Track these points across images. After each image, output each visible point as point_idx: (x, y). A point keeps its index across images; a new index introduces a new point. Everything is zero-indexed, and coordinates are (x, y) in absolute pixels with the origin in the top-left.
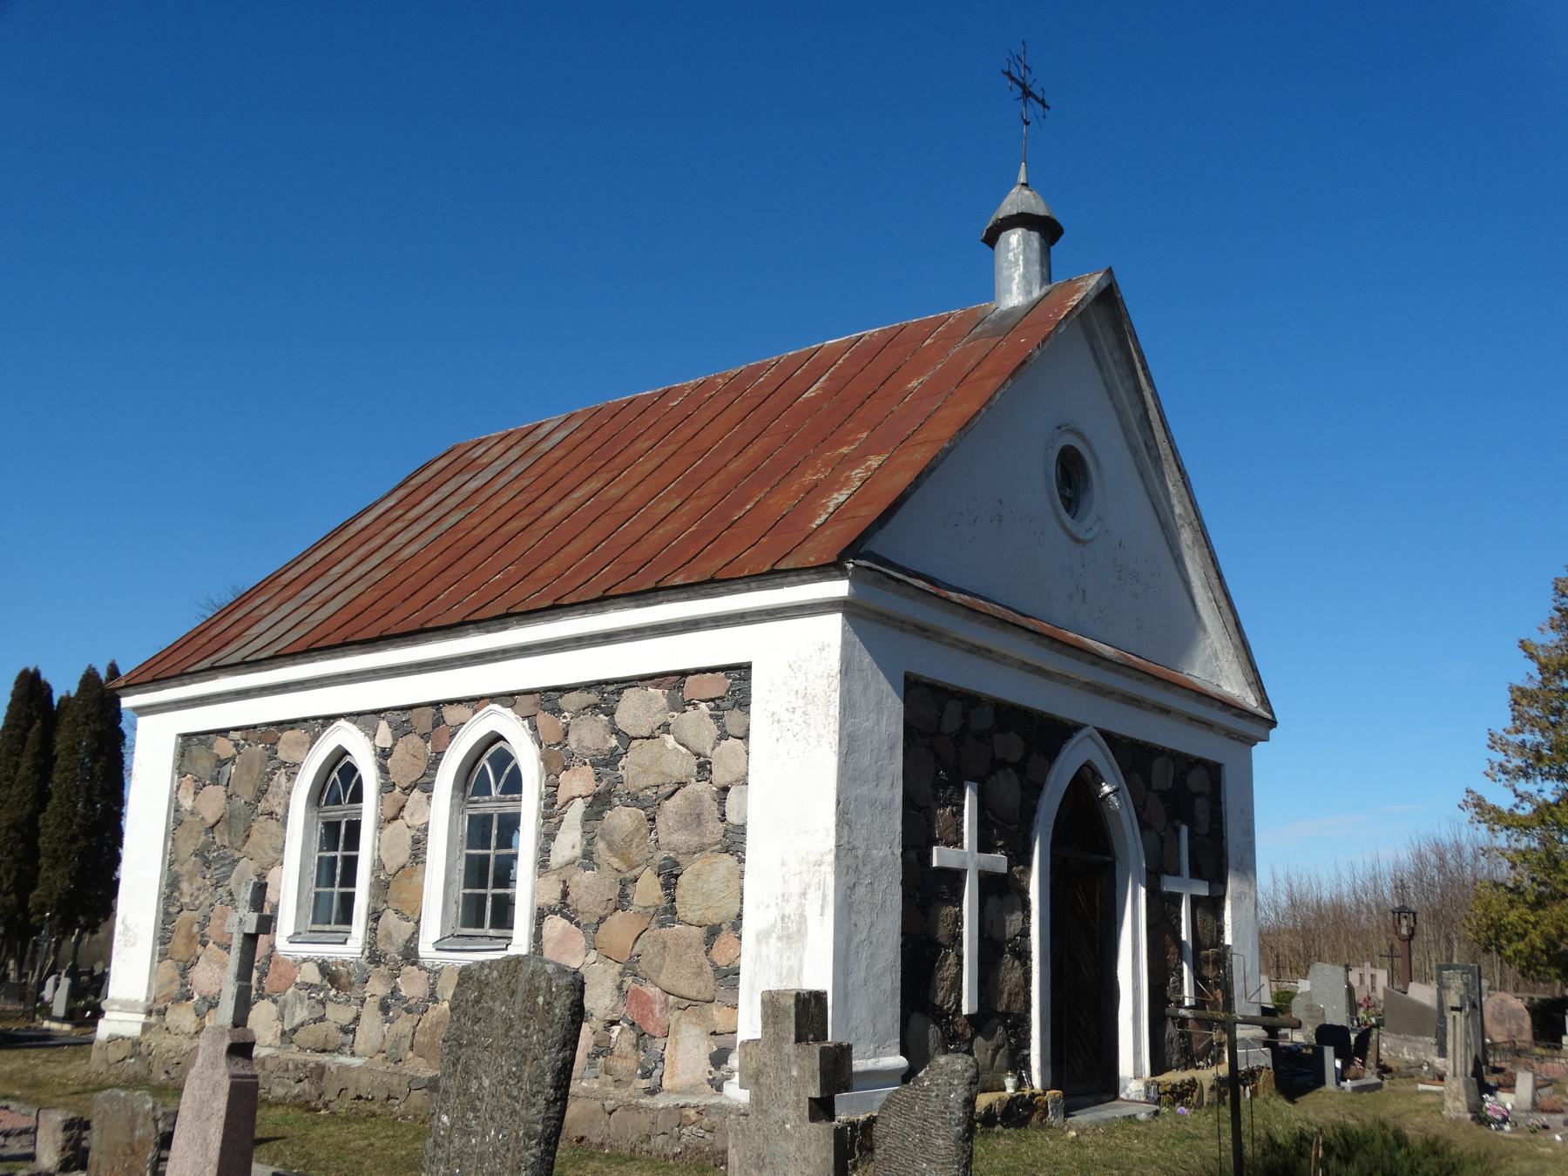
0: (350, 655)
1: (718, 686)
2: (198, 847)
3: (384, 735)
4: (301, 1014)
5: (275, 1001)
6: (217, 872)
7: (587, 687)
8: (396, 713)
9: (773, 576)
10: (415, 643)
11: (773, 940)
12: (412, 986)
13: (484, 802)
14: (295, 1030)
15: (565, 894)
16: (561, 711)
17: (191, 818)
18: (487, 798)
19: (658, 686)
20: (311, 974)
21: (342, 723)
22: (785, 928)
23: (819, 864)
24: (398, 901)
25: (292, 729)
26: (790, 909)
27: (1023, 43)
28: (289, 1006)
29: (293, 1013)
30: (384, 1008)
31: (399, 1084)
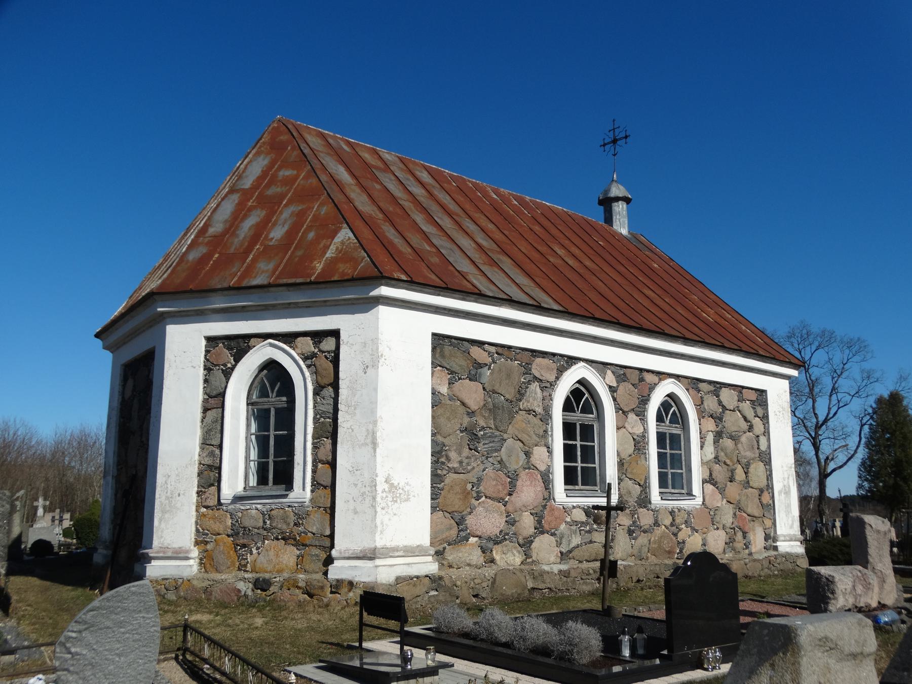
0: (574, 321)
1: (753, 396)
2: (464, 425)
3: (611, 378)
4: (576, 540)
5: (553, 534)
6: (486, 446)
7: (710, 382)
8: (617, 368)
9: (686, 341)
10: (649, 337)
11: (783, 494)
12: (646, 518)
13: (663, 426)
14: (570, 552)
15: (711, 474)
16: (699, 391)
17: (449, 402)
18: (663, 424)
19: (734, 390)
20: (580, 516)
21: (582, 364)
22: (785, 490)
23: (791, 468)
24: (631, 473)
25: (543, 357)
26: (786, 483)
27: (614, 120)
28: (566, 536)
29: (570, 540)
30: (630, 532)
31: (660, 570)
